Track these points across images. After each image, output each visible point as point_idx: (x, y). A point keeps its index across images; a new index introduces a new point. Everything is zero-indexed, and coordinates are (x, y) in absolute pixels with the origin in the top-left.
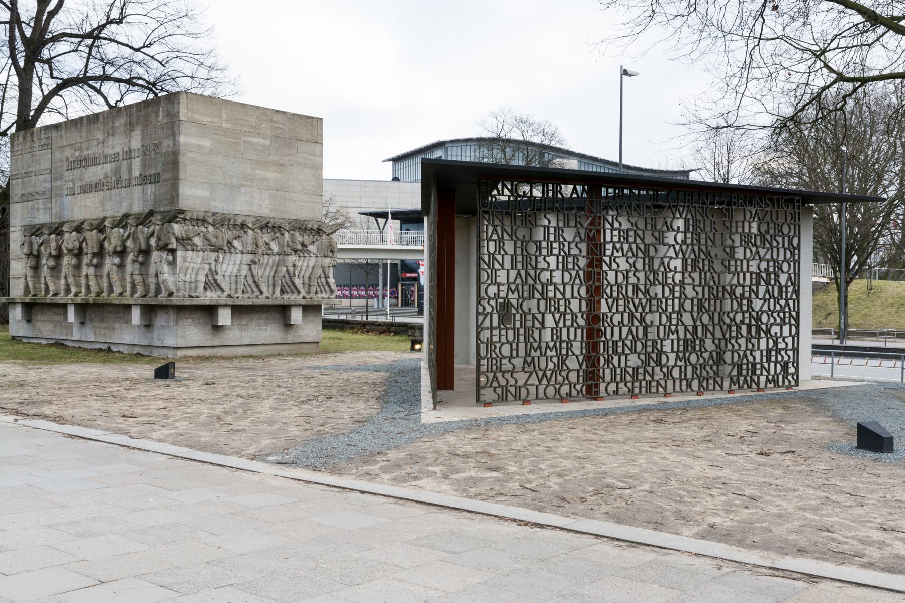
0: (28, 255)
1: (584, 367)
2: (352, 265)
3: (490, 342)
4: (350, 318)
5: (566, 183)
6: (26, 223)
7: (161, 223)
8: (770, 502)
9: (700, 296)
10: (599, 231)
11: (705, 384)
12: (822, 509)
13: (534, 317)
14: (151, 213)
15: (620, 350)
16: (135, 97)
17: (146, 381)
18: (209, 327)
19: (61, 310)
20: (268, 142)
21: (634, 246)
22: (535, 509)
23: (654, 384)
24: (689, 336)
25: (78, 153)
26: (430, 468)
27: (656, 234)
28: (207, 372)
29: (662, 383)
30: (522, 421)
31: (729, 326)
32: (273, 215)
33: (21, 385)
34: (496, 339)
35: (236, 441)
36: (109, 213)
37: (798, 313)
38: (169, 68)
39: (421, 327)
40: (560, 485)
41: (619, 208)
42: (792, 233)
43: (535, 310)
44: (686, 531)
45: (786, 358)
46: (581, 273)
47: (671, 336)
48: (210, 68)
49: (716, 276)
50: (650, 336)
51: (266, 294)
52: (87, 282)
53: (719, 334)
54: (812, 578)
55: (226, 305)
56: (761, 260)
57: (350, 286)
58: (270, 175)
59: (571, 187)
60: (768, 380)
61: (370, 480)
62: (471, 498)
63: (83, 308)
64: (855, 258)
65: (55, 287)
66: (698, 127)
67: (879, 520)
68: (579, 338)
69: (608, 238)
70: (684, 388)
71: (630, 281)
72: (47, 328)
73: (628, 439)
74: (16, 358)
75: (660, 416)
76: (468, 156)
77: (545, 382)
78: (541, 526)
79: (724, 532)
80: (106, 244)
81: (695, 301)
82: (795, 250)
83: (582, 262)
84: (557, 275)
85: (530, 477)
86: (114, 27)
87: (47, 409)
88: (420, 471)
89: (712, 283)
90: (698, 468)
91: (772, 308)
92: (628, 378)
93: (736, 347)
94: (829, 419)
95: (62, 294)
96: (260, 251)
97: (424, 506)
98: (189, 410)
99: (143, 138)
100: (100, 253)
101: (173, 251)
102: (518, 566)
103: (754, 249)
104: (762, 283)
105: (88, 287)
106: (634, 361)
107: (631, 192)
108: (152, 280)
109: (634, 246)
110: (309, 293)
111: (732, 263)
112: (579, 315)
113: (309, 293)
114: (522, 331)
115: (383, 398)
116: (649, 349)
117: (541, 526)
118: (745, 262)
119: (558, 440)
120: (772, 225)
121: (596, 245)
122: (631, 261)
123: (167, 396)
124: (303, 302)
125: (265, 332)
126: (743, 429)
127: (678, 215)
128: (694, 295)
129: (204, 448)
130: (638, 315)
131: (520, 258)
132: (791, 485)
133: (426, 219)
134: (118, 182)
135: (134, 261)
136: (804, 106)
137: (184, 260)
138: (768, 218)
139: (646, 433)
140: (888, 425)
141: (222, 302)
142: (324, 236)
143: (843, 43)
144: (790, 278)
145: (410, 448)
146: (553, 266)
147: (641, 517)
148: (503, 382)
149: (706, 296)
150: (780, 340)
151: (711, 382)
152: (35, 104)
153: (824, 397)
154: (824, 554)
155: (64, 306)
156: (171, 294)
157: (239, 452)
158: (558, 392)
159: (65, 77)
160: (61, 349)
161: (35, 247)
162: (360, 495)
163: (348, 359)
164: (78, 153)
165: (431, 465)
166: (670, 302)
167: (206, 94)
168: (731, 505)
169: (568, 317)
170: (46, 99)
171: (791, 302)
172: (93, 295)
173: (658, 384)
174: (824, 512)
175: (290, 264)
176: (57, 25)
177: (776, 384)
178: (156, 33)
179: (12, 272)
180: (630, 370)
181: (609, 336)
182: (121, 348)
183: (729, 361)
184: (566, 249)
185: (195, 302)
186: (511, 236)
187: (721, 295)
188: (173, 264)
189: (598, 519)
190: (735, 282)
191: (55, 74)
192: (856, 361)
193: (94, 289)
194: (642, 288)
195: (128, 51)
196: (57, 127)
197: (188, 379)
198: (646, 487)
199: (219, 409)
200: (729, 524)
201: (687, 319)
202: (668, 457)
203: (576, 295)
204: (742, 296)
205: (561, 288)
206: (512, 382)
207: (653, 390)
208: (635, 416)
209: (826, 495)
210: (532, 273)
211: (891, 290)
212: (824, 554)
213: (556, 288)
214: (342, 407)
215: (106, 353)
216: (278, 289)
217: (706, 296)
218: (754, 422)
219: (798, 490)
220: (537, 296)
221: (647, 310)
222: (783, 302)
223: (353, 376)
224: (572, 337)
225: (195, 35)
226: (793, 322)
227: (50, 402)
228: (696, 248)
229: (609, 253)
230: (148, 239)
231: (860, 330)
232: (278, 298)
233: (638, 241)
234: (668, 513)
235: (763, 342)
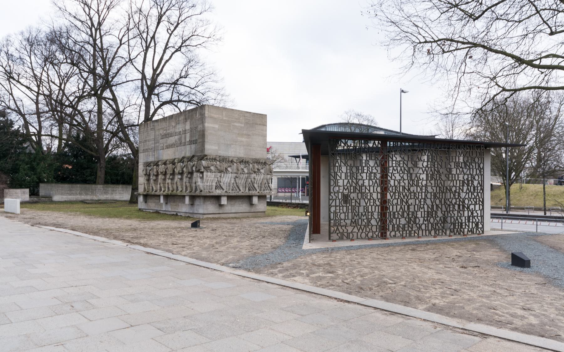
0: (145, 175)
1: (379, 224)
2: (285, 178)
3: (335, 212)
4: (284, 201)
6: (145, 161)
7: (197, 161)
8: (464, 293)
9: (435, 191)
10: (386, 162)
11: (437, 232)
12: (491, 297)
13: (356, 201)
14: (193, 156)
15: (396, 216)
18: (218, 205)
19: (158, 198)
20: (243, 125)
21: (403, 168)
22: (347, 293)
23: (413, 232)
24: (429, 210)
25: (165, 132)
26: (302, 271)
27: (413, 163)
28: (214, 225)
29: (417, 232)
30: (348, 249)
31: (449, 205)
34: (338, 211)
35: (218, 256)
36: (177, 157)
37: (483, 199)
38: (205, 96)
41: (395, 151)
42: (480, 162)
44: (421, 307)
45: (477, 220)
46: (378, 181)
47: (421, 210)
48: (222, 95)
49: (442, 182)
50: (411, 210)
53: (444, 209)
54: (484, 335)
55: (225, 196)
56: (464, 174)
57: (285, 188)
59: (373, 142)
61: (272, 277)
62: (317, 286)
63: (167, 197)
64: (514, 173)
65: (155, 188)
66: (435, 114)
67: (521, 304)
68: (377, 210)
70: (427, 234)
71: (401, 184)
72: (152, 205)
73: (398, 259)
75: (414, 247)
76: (335, 129)
77: (361, 231)
78: (348, 302)
79: (439, 308)
81: (433, 194)
82: (481, 170)
83: (378, 176)
85: (347, 276)
87: (142, 241)
88: (296, 273)
89: (440, 185)
90: (431, 274)
91: (470, 197)
92: (401, 229)
93: (453, 215)
94: (498, 250)
95: (158, 191)
96: (239, 172)
97: (295, 290)
98: (201, 242)
99: (190, 125)
100: (173, 174)
101: (202, 173)
102: (333, 324)
103: (461, 169)
104: (465, 185)
105: (169, 188)
106: (403, 221)
107: (401, 144)
108: (194, 185)
109: (403, 168)
110: (261, 190)
111: (451, 176)
112: (377, 200)
113: (261, 190)
115: (287, 238)
116: (410, 216)
117: (348, 302)
118: (457, 176)
119: (364, 259)
120: (470, 158)
124: (258, 194)
125: (242, 207)
126: (454, 254)
127: (424, 154)
128: (432, 191)
129: (202, 259)
130: (405, 200)
132: (476, 284)
134: (181, 143)
135: (186, 177)
136: (486, 104)
137: (207, 176)
138: (468, 155)
139: (407, 256)
140: (528, 254)
141: (223, 194)
143: (505, 73)
144: (479, 183)
145: (294, 261)
146: (365, 178)
147: (399, 299)
148: (341, 231)
149: (438, 191)
150: (474, 212)
151: (441, 231)
152: (151, 112)
153: (496, 239)
154: (491, 322)
155: (159, 196)
156: (201, 191)
157: (217, 262)
158: (367, 235)
159: (163, 101)
160: (158, 215)
161: (148, 171)
162: (266, 284)
164: (165, 132)
165: (302, 270)
166: (420, 194)
167: (221, 106)
168: (444, 294)
169: (372, 201)
171: (480, 194)
173: (415, 232)
174: (492, 299)
176: (160, 80)
177: (473, 233)
178: (201, 81)
179: (139, 182)
180: (401, 226)
181: (391, 210)
182: (182, 214)
183: (449, 222)
184: (370, 170)
185: (211, 194)
186: (345, 165)
187: (445, 191)
188: (202, 178)
189: (377, 299)
190: (452, 184)
191: (160, 100)
192: (514, 221)
193: (171, 189)
194: (407, 188)
197: (205, 228)
198: (403, 283)
200: (442, 303)
201: (429, 202)
202: (416, 268)
203: (375, 191)
204: (455, 191)
206: (345, 231)
207: (413, 235)
208: (402, 247)
209: (494, 289)
210: (355, 181)
211: (531, 188)
212: (491, 322)
213: (366, 188)
214: (268, 241)
215: (175, 216)
216: (247, 189)
217: (438, 191)
218: (460, 251)
219: (479, 287)
220: (357, 191)
221: (409, 198)
222: (475, 194)
223: (276, 227)
224: (373, 210)
225: (216, 82)
226: (481, 203)
227: (144, 237)
228: (433, 169)
229: (391, 171)
231: (516, 207)
232: (247, 192)
233: (405, 166)
234: (412, 297)
235: (466, 214)
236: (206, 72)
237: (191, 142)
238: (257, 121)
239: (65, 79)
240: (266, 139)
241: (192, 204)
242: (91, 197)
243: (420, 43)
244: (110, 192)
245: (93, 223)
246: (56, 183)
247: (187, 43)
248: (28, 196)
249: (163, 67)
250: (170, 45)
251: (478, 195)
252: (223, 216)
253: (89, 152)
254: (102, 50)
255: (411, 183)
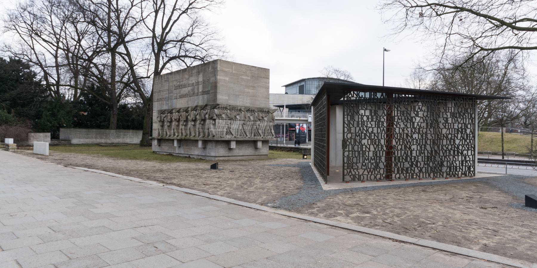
3: (348, 156)
5: (379, 92)
6: (159, 109)
7: (211, 109)
10: (392, 112)
14: (206, 105)
15: (401, 160)
16: (197, 63)
17: (207, 170)
19: (171, 142)
20: (249, 78)
23: (415, 174)
24: (429, 155)
27: (416, 113)
29: (418, 174)
31: (446, 151)
32: (251, 106)
33: (161, 171)
34: (350, 155)
35: (252, 197)
36: (190, 105)
38: (209, 52)
39: (310, 149)
40: (400, 221)
43: (366, 144)
46: (385, 129)
48: (224, 52)
49: (440, 130)
51: (249, 136)
52: (181, 131)
53: (441, 154)
56: (459, 123)
58: (250, 91)
60: (462, 174)
63: (180, 141)
65: (169, 133)
68: (384, 155)
69: (396, 114)
70: (427, 176)
72: (166, 148)
74: (156, 160)
77: (370, 173)
80: (189, 117)
84: (375, 129)
86: (188, 38)
87: (175, 181)
92: (404, 172)
93: (449, 159)
95: (172, 136)
96: (247, 120)
99: (203, 77)
100: (187, 121)
101: (215, 120)
105: (182, 133)
106: (407, 165)
108: (206, 131)
111: (447, 124)
113: (264, 136)
114: (361, 152)
116: (413, 160)
121: (391, 117)
122: (405, 124)
123: (218, 176)
124: (262, 139)
125: (248, 151)
130: (408, 146)
131: (360, 123)
133: (312, 107)
135: (200, 124)
137: (219, 123)
138: (461, 106)
141: (233, 139)
142: (270, 114)
144: (471, 131)
148: (353, 173)
151: (438, 174)
152: (160, 66)
155: (173, 140)
156: (214, 136)
157: (255, 202)
158: (375, 177)
160: (172, 157)
161: (162, 118)
163: (280, 161)
169: (380, 146)
170: (165, 64)
171: (472, 141)
172: (184, 136)
175: (257, 125)
176: (169, 37)
178: (204, 40)
180: (405, 169)
182: (194, 156)
185: (223, 139)
188: (214, 124)
190: (448, 132)
193: (184, 134)
194: (410, 135)
195: (194, 46)
196: (167, 74)
197: (223, 169)
199: (240, 182)
201: (428, 147)
204: (451, 138)
205: (377, 135)
206: (357, 173)
210: (365, 128)
213: (375, 135)
215: (188, 158)
216: (253, 134)
220: (367, 138)
222: (468, 141)
224: (381, 155)
225: (218, 40)
227: (174, 178)
229: (396, 120)
230: (205, 115)
232: (253, 138)
233: (408, 115)
235: (460, 157)
236: (209, 31)
237: (204, 93)
238: (261, 75)
239: (81, 35)
240: (269, 91)
241: (204, 148)
242: (105, 140)
243: (412, 7)
244: (122, 136)
245: (119, 164)
246: (73, 127)
247: (194, 5)
248: (50, 139)
249: (172, 26)
250: (177, 7)
251: (470, 142)
252: (231, 158)
253: (104, 101)
254: (117, 10)
255: (413, 130)
